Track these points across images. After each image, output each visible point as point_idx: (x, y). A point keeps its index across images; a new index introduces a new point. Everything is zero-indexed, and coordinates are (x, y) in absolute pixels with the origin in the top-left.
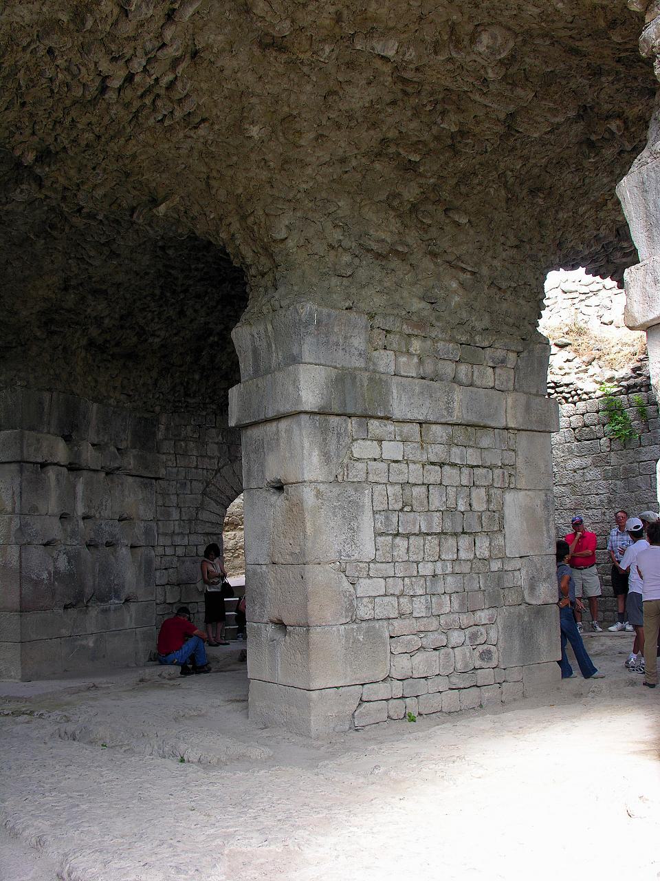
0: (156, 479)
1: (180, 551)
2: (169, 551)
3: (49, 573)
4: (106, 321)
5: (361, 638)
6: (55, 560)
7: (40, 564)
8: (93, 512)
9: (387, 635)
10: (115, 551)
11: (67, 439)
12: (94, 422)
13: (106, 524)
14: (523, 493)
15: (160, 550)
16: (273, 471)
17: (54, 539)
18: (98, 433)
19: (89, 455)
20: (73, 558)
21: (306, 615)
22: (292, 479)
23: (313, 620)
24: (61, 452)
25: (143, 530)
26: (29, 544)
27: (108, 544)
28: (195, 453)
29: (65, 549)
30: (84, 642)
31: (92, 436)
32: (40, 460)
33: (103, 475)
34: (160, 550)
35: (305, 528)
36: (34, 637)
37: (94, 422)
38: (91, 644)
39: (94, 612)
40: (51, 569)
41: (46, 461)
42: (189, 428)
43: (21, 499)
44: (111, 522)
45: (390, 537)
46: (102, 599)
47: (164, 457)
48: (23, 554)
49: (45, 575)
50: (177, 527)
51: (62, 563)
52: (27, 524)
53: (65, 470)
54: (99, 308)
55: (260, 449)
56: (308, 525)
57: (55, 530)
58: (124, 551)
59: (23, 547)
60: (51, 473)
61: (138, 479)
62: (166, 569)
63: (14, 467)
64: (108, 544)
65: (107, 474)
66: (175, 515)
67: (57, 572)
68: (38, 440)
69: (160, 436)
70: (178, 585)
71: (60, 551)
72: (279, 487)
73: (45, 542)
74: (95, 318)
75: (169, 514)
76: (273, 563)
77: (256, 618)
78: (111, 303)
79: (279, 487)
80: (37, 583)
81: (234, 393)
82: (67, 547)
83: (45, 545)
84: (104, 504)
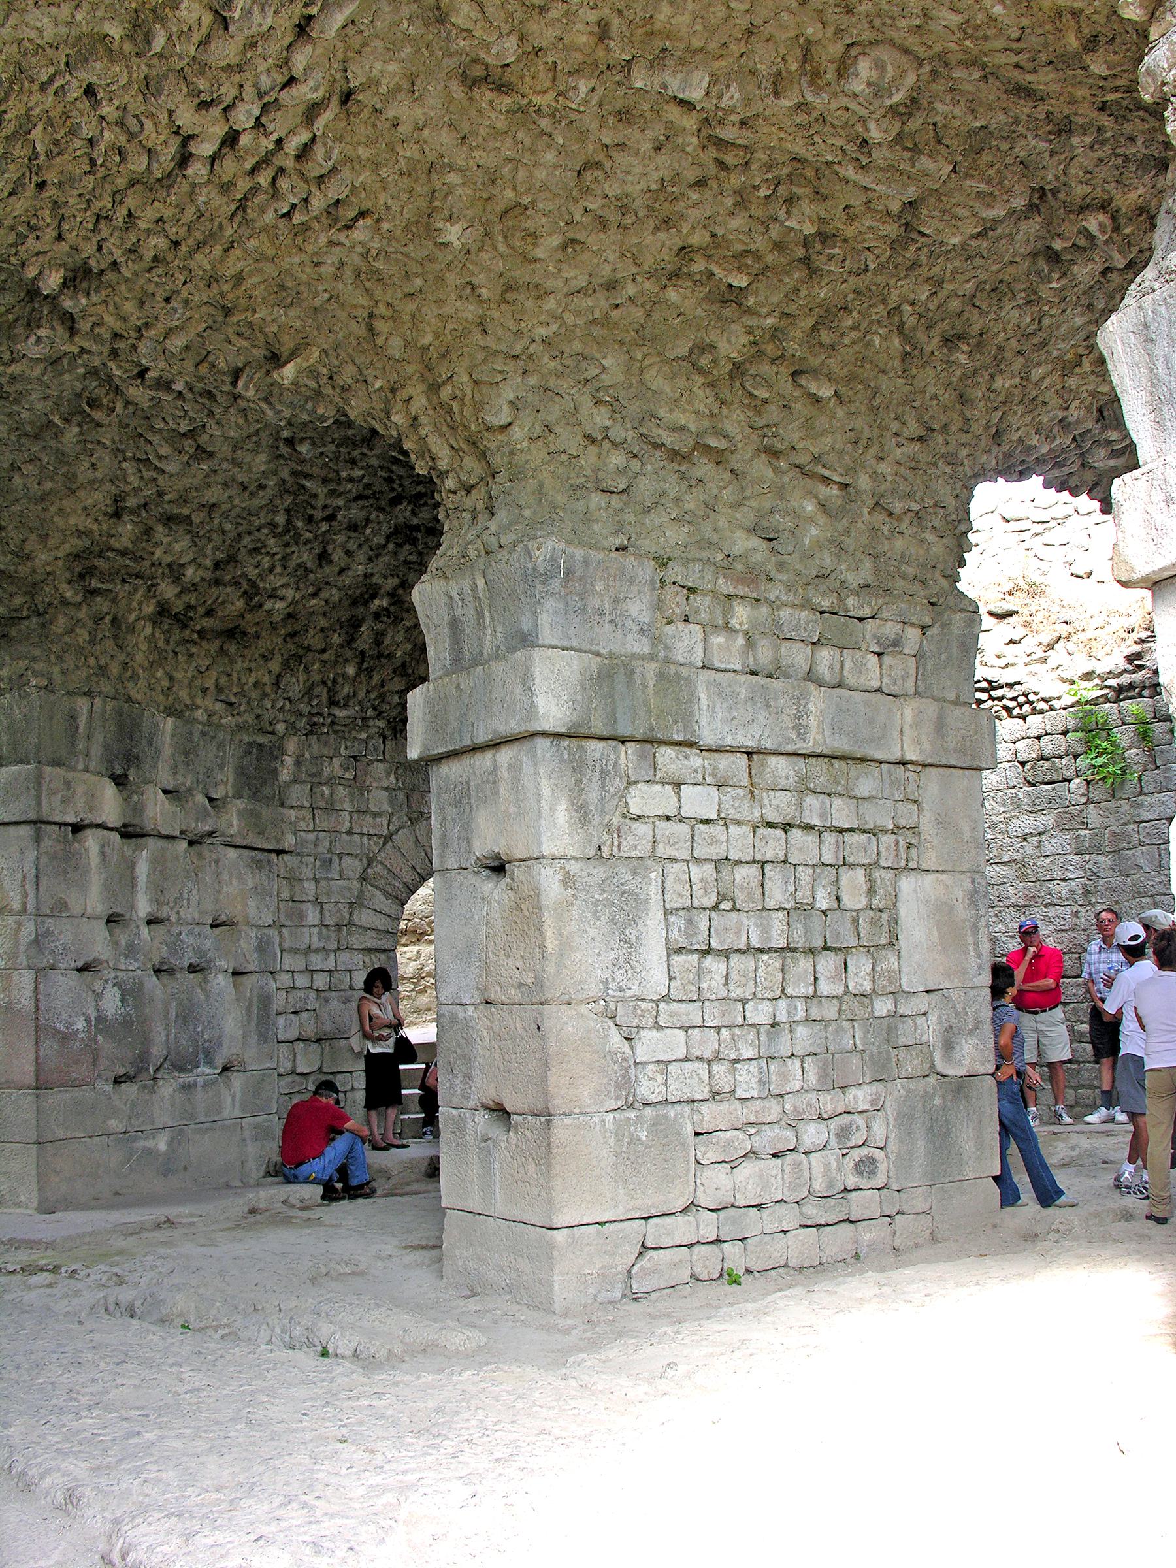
0: (279, 852)
2: (301, 981)
3: (88, 1020)
6: (98, 997)
8: (165, 912)
9: (689, 1130)
12: (167, 751)
20: (131, 993)
21: (546, 1095)
24: (109, 805)
26: (52, 967)
27: (193, 969)
28: (347, 806)
30: (150, 1143)
33: (184, 845)
36: (61, 1133)
37: (167, 751)
38: (162, 1147)
39: (167, 1088)
44: (197, 929)
45: (695, 956)
48: (41, 987)
49: (80, 1024)
50: (315, 939)
52: (48, 933)
53: (115, 836)
54: (177, 547)
56: (549, 934)
58: (221, 981)
61: (246, 852)
62: (295, 1013)
64: (193, 969)
66: (312, 915)
69: (285, 775)
70: (318, 1041)
72: (498, 868)
73: (80, 964)
74: (169, 565)
75: (301, 916)
82: (120, 974)
83: (80, 970)
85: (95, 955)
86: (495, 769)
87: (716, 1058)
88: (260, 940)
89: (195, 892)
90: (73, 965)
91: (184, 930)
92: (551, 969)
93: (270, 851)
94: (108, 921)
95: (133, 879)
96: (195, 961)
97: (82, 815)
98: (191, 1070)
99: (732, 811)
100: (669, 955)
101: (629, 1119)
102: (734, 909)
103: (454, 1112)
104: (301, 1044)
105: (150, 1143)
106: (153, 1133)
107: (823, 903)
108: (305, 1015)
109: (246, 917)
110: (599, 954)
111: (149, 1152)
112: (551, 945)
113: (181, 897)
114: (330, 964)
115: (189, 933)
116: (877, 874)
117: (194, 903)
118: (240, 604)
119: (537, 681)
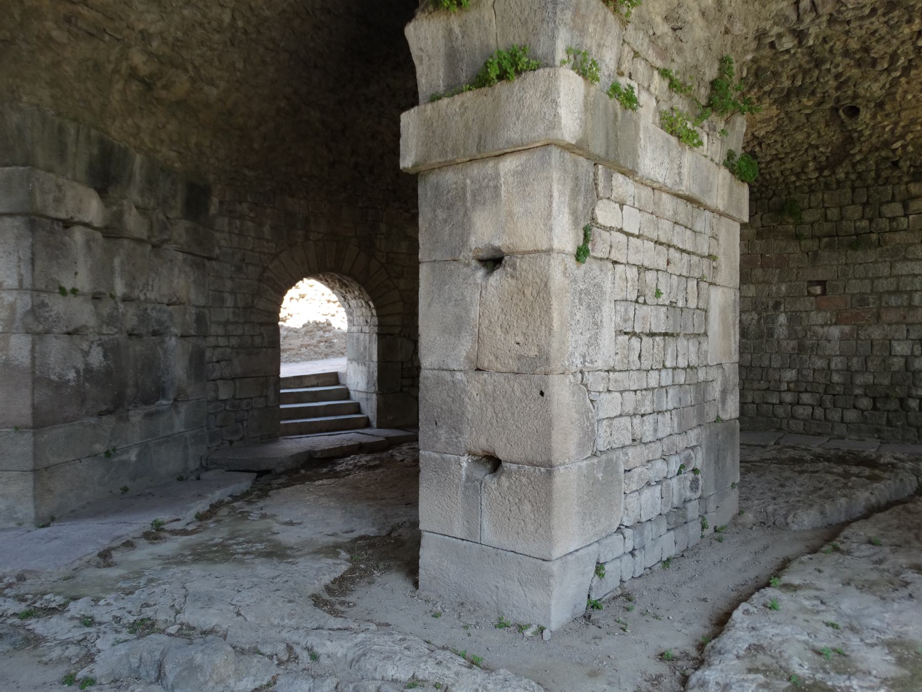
0: (210, 259)
1: (234, 341)
2: (222, 341)
3: (78, 372)
4: (155, 44)
5: (600, 476)
6: (86, 354)
7: (61, 359)
8: (136, 293)
9: (622, 470)
10: (163, 342)
11: (102, 192)
12: (138, 177)
13: (153, 309)
14: (721, 289)
15: (211, 341)
16: (484, 233)
17: (84, 326)
18: (142, 193)
19: (133, 222)
20: (111, 350)
21: (549, 450)
22: (526, 244)
23: (556, 457)
24: (93, 209)
25: (194, 317)
26: (48, 332)
27: (155, 333)
28: (252, 234)
29: (100, 339)
30: (124, 457)
31: (134, 195)
32: (62, 215)
33: (149, 247)
34: (211, 341)
35: (551, 320)
36: (53, 460)
37: (138, 177)
38: (133, 458)
39: (136, 416)
40: (81, 366)
41: (72, 218)
42: (245, 205)
43: (33, 269)
44: (158, 306)
45: (627, 337)
46: (147, 400)
47: (217, 235)
48: (37, 347)
49: (72, 375)
50: (231, 316)
51: (96, 358)
52: (43, 305)
53: (99, 235)
54: (149, 17)
55: (458, 207)
56: (555, 315)
57: (83, 313)
58: (172, 342)
59: (38, 336)
60: (78, 235)
61: (190, 257)
62: (218, 362)
63: (18, 222)
64: (155, 333)
65: (154, 246)
66: (229, 302)
67: (88, 370)
68: (59, 187)
69: (213, 210)
70: (233, 379)
71: (92, 342)
72: (493, 261)
73: (70, 329)
74: (141, 32)
75: (223, 300)
76: (478, 369)
77: (438, 446)
78: (164, 15)
79: (493, 261)
80: (61, 385)
81: (409, 120)
82: (102, 337)
83: (69, 334)
84: (151, 283)
85: (83, 322)
86: (497, 176)
87: (635, 415)
88: (198, 315)
89: (157, 280)
90: (65, 330)
91: (149, 306)
92: (555, 345)
93: (204, 257)
94: (94, 298)
95: (112, 267)
96: (157, 328)
97: (72, 214)
98: (153, 403)
99: (646, 230)
100: (616, 336)
101: (594, 464)
102: (645, 303)
103: (436, 455)
104: (222, 382)
105: (124, 457)
106: (126, 451)
107: (680, 304)
108: (223, 363)
109: (189, 300)
110: (581, 333)
111: (124, 463)
112: (556, 325)
113: (147, 284)
114: (240, 331)
115: (153, 309)
116: (702, 284)
117: (156, 288)
118: (187, 85)
119: (562, 94)
